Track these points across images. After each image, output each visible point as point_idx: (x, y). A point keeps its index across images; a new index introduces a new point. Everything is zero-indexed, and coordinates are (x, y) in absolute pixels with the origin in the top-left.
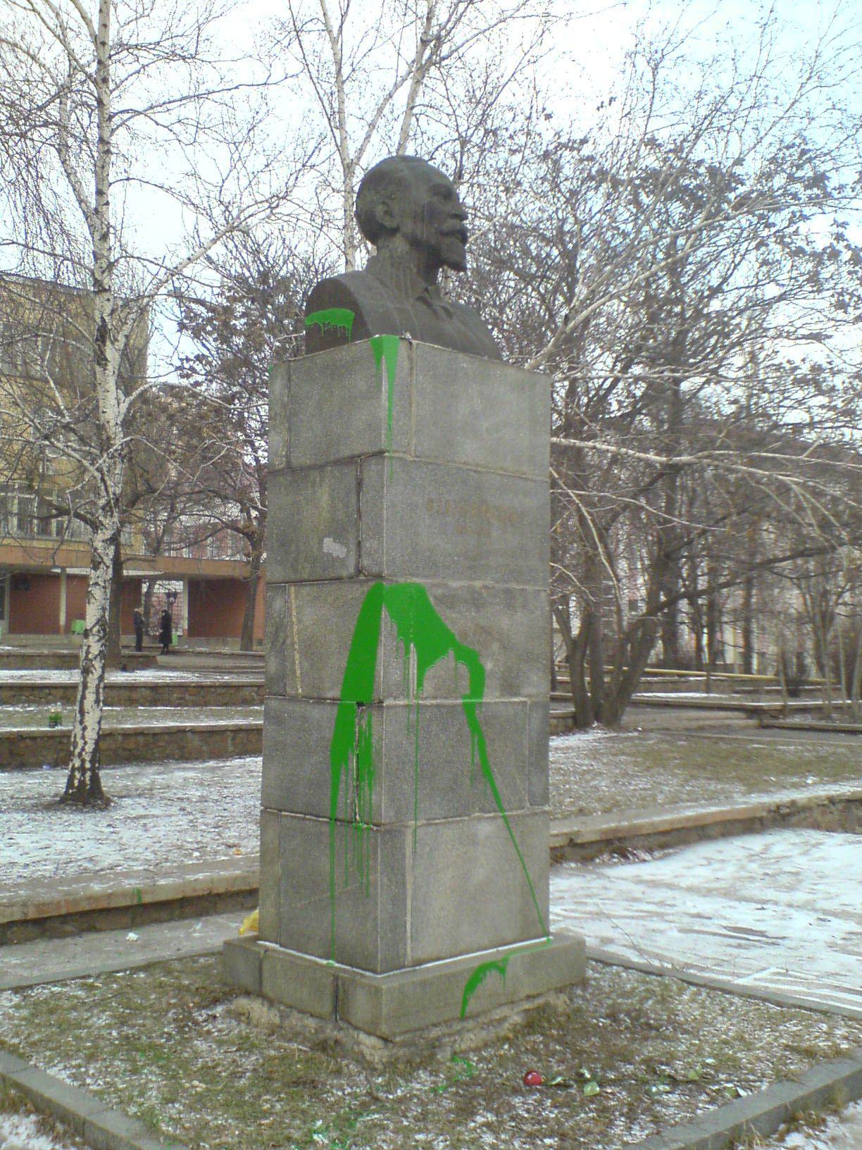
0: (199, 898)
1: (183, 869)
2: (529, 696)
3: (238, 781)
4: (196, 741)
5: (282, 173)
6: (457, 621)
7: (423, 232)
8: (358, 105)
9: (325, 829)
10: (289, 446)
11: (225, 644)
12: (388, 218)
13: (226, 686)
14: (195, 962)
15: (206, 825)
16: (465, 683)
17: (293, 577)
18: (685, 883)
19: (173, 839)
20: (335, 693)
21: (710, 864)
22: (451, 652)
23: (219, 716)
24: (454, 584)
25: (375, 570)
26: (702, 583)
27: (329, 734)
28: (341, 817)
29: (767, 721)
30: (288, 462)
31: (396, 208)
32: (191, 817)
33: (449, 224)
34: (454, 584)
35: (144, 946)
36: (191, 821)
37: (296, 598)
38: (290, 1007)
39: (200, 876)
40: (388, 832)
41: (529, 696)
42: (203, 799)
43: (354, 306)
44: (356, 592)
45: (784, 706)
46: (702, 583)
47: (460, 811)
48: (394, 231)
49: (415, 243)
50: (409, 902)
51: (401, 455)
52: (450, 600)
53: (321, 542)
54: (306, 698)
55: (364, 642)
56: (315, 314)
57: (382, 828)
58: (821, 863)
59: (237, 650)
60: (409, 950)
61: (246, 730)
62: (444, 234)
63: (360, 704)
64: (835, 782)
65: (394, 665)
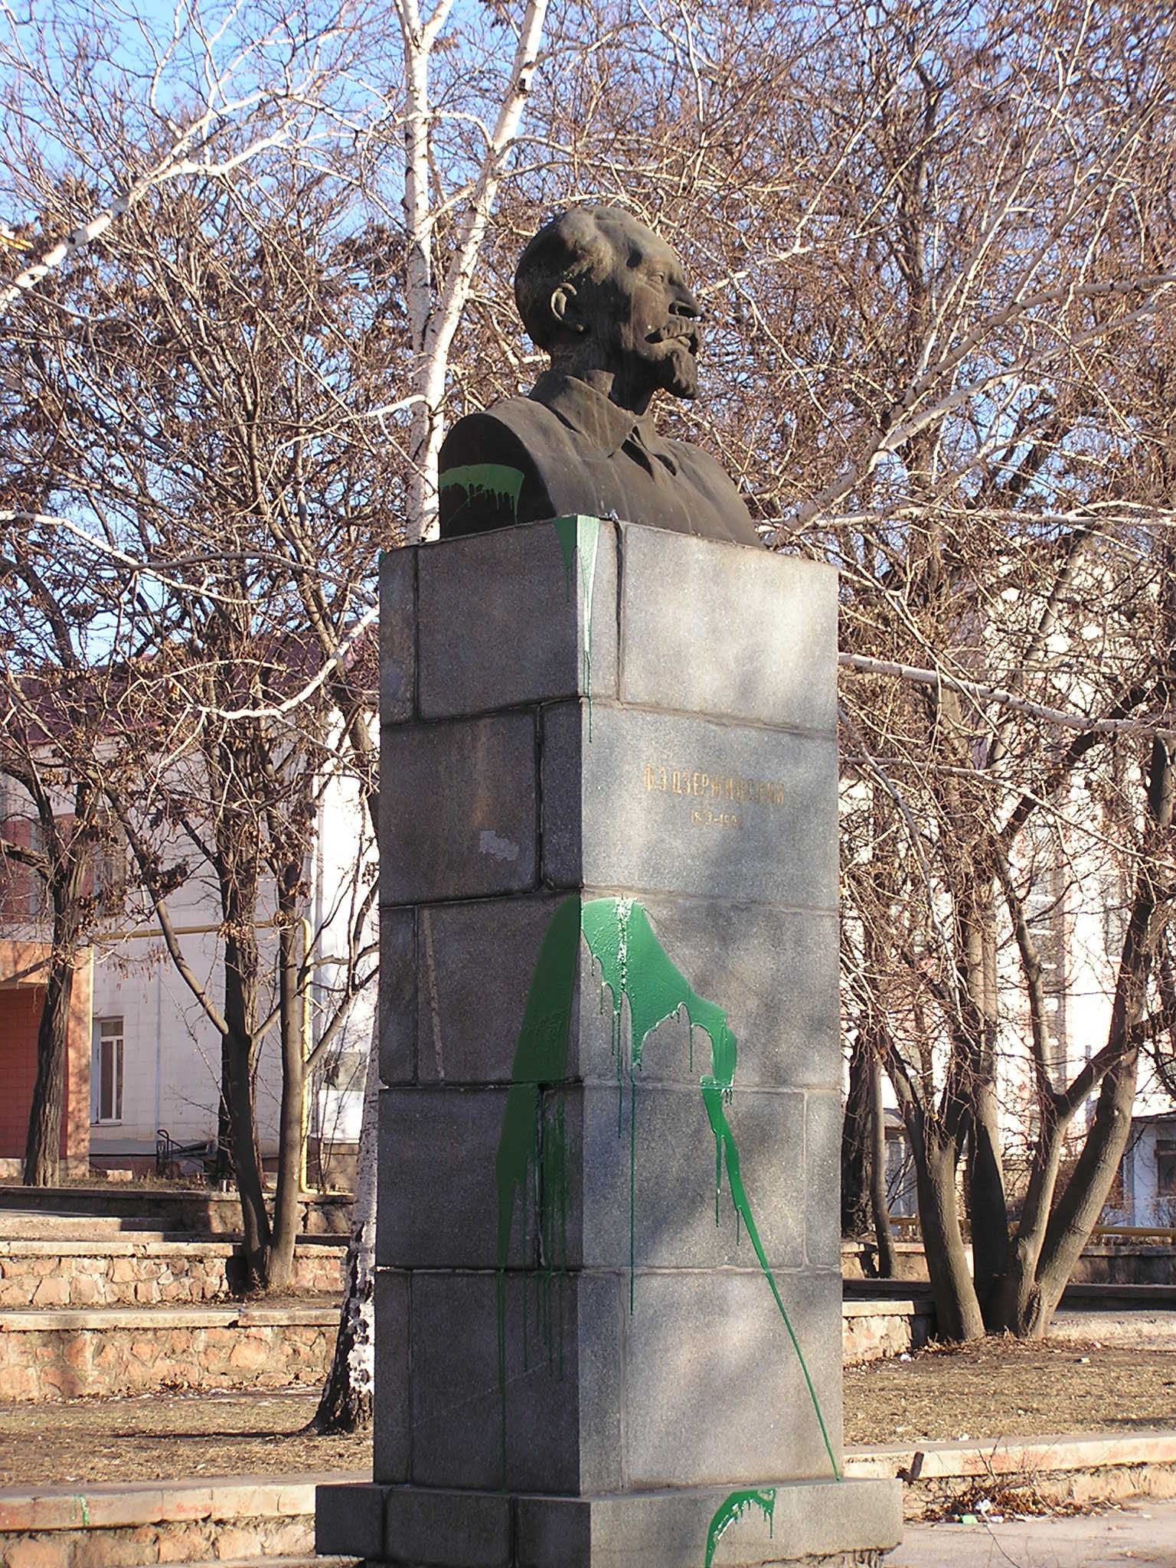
30: (417, 709)
63: (543, 1087)
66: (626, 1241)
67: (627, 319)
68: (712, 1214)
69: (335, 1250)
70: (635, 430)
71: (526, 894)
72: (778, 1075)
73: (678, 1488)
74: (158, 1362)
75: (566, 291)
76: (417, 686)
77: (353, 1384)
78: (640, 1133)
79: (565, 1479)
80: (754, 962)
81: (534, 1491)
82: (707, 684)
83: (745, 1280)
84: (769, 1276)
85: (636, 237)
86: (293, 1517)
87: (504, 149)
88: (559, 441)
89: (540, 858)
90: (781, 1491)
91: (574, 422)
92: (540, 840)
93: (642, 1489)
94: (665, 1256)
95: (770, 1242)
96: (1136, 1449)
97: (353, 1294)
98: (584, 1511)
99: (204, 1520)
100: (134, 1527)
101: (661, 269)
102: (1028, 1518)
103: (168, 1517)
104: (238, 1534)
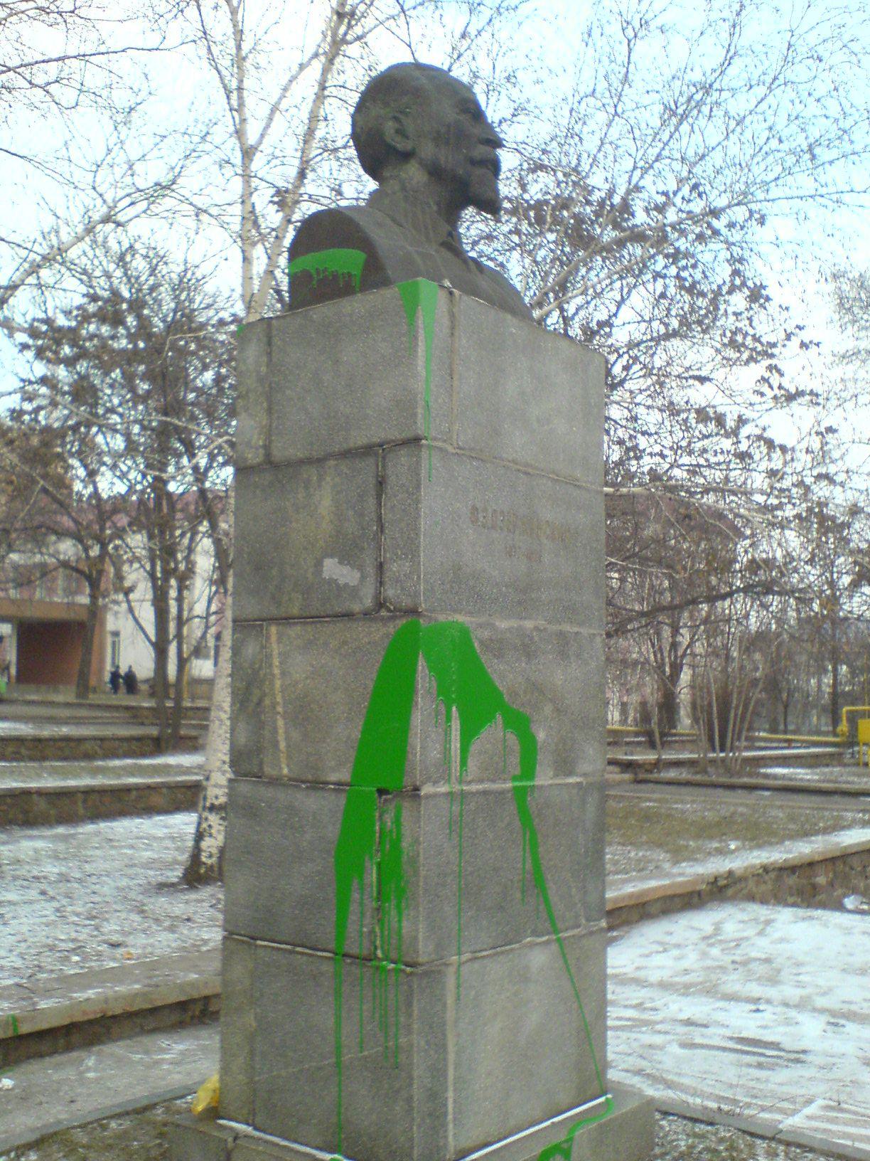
0: (90, 1022)
1: (67, 982)
2: (585, 775)
3: (98, 852)
4: (42, 804)
5: (173, 152)
6: (506, 674)
7: (447, 158)
8: (261, 88)
9: (326, 967)
10: (269, 433)
11: (56, 691)
12: (398, 139)
13: (67, 739)
14: (104, 1128)
15: (78, 915)
16: (515, 760)
17: (274, 612)
18: (654, 977)
19: (42, 936)
20: (343, 775)
21: (665, 951)
22: (499, 718)
23: (65, 774)
24: (503, 624)
25: (406, 602)
27: (332, 832)
28: (354, 951)
29: (641, 776)
30: (268, 455)
31: (410, 127)
32: (55, 904)
33: (480, 151)
34: (503, 624)
35: (24, 1097)
36: (58, 910)
37: (279, 641)
39: (91, 993)
40: (426, 974)
41: (585, 775)
42: (64, 878)
43: (366, 244)
44: (378, 632)
45: (658, 760)
47: (508, 939)
48: (407, 156)
49: (435, 172)
50: (451, 1073)
51: (440, 444)
52: (497, 647)
53: (319, 564)
54: (295, 782)
55: (388, 707)
56: (303, 258)
57: (420, 970)
58: (783, 946)
59: (71, 698)
60: (450, 1139)
61: (98, 792)
62: (473, 162)
63: (381, 792)
64: (759, 847)
65: (432, 736)
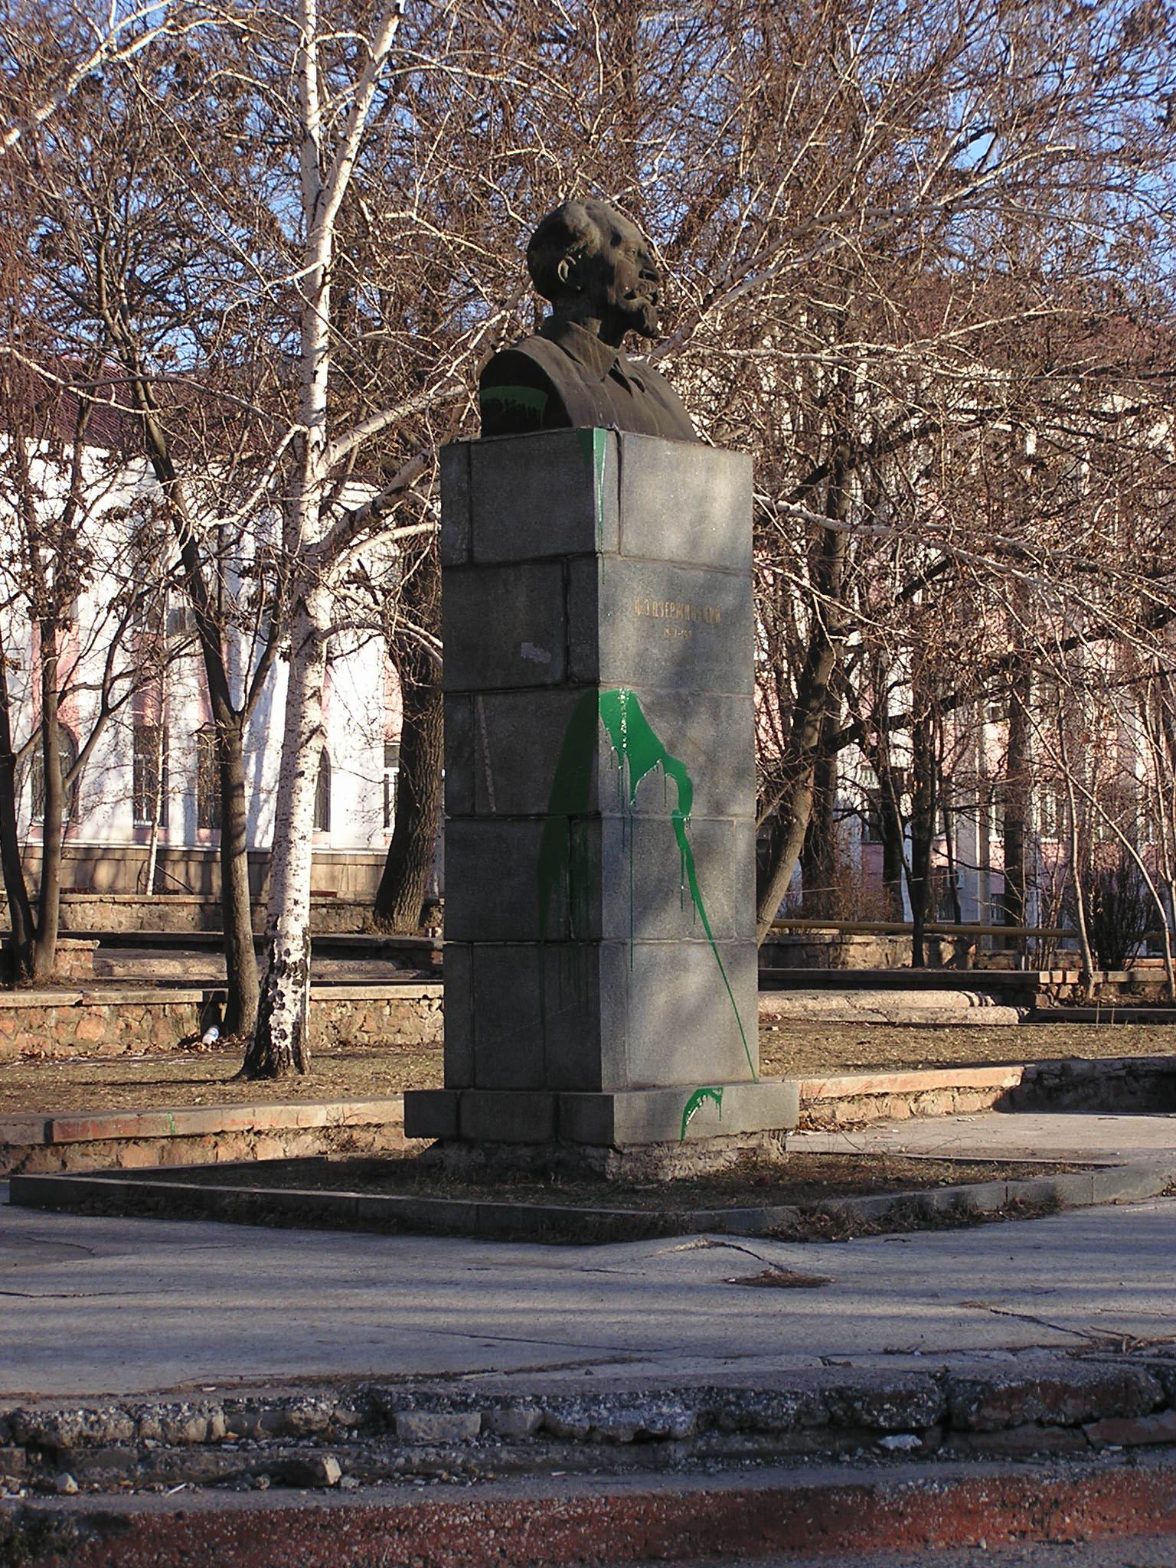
26: (899, 702)
38: (498, 1142)
46: (899, 702)
63: (570, 818)
66: (628, 921)
67: (611, 283)
68: (679, 903)
69: (89, 944)
70: (617, 361)
71: (557, 686)
72: (718, 807)
73: (660, 1088)
74: (19, 1036)
75: (569, 262)
76: (471, 541)
77: (274, 1041)
78: (635, 849)
79: (593, 1080)
80: (701, 730)
81: (567, 1089)
82: (672, 542)
83: (699, 947)
84: (713, 944)
85: (616, 224)
86: (305, 1129)
87: (381, 60)
88: (568, 369)
89: (568, 662)
90: (726, 1088)
91: (576, 356)
92: (567, 651)
93: (639, 1087)
94: (650, 930)
95: (714, 920)
96: (881, 1083)
97: (271, 971)
98: (609, 1100)
99: (248, 1131)
100: (201, 1136)
101: (634, 247)
102: (810, 1133)
103: (226, 1129)
104: (269, 1141)
